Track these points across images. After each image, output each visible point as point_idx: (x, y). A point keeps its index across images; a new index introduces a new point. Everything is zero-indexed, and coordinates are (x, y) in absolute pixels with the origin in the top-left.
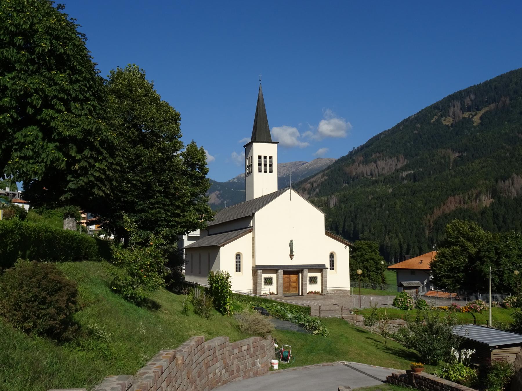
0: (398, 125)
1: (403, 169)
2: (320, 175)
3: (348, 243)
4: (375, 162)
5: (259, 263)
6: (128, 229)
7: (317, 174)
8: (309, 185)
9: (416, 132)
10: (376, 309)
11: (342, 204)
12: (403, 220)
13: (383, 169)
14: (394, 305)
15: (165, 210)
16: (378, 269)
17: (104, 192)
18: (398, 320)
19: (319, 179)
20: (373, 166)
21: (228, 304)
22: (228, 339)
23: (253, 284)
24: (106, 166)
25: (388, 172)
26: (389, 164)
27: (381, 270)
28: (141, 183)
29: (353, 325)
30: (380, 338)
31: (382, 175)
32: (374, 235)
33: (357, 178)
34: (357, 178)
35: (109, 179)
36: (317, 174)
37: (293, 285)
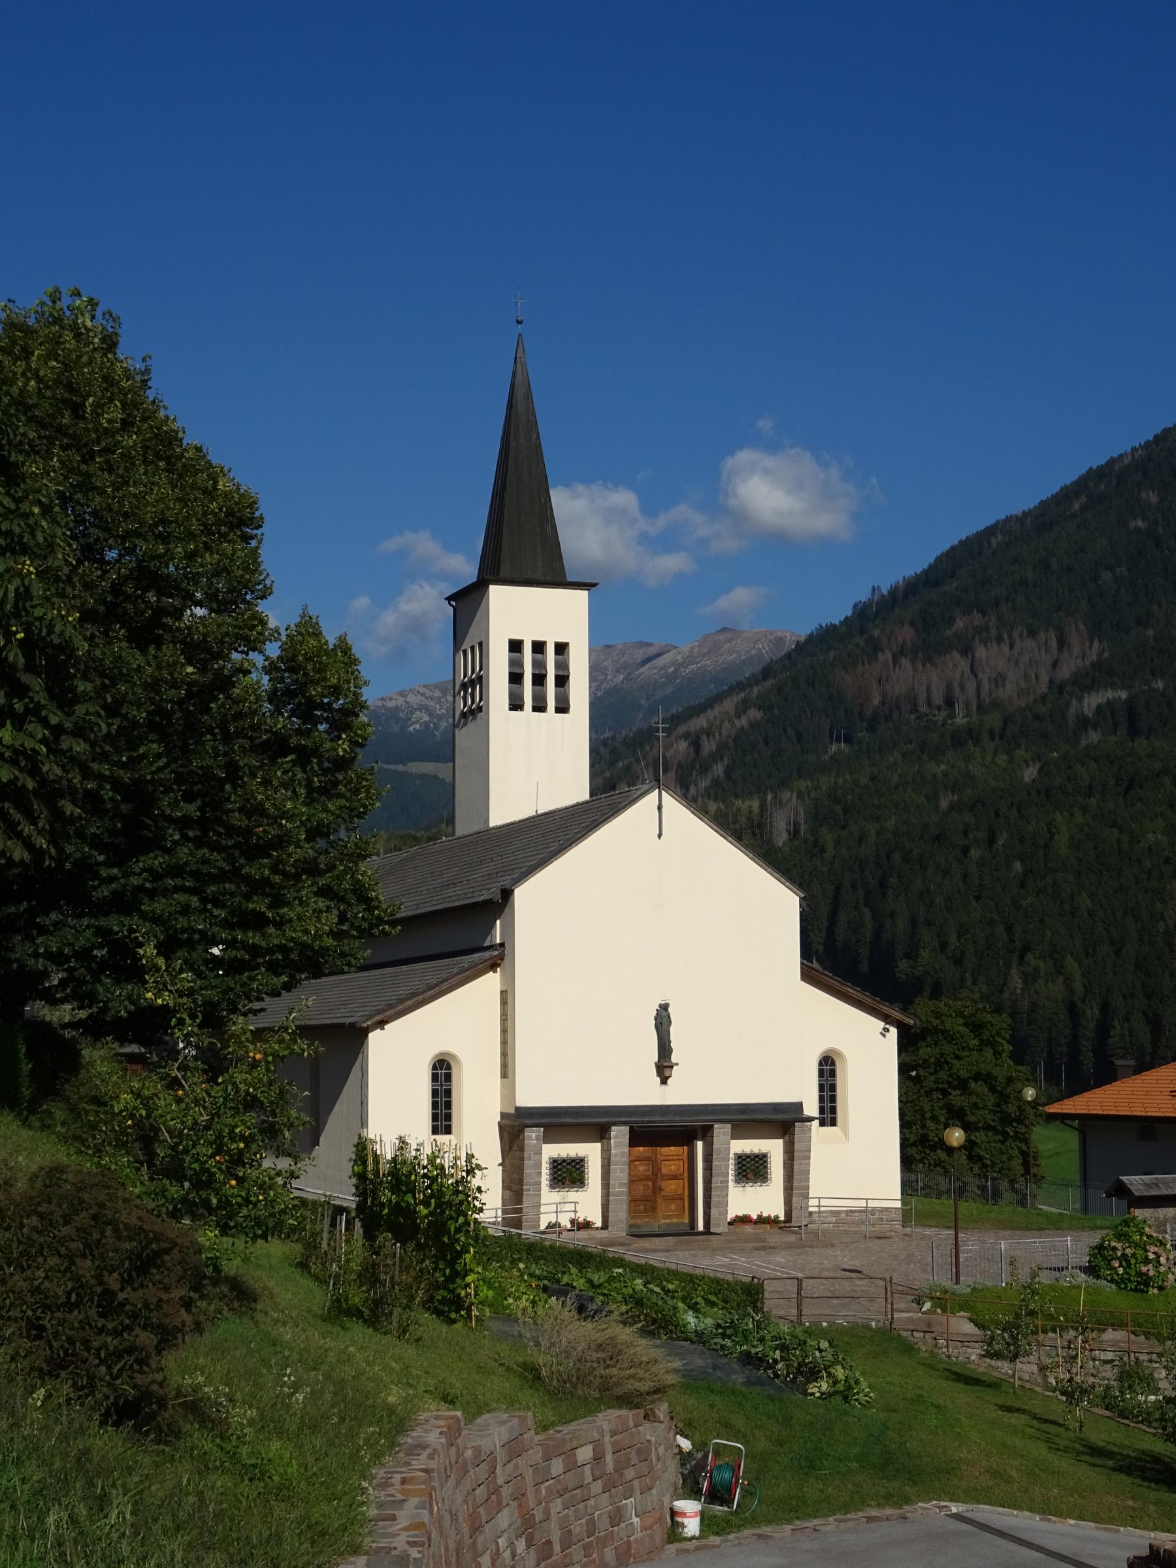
0: (1065, 496)
1: (1086, 682)
2: (729, 705)
3: (897, 1015)
4: (966, 650)
5: (528, 1097)
6: (157, 996)
7: (718, 698)
8: (683, 746)
9: (1140, 524)
10: (1034, 1292)
11: (824, 830)
12: (1085, 901)
13: (999, 680)
14: (1091, 1270)
15: (204, 900)
16: (1006, 1119)
17: (29, 845)
18: (1110, 1335)
19: (728, 719)
20: (955, 665)
21: (469, 1279)
22: (530, 1422)
23: (505, 1187)
24: (44, 741)
25: (1021, 693)
26: (1026, 658)
27: (1020, 1121)
28: (117, 785)
29: (933, 1355)
30: (1057, 1406)
31: (996, 704)
32: (958, 961)
33: (888, 718)
34: (888, 718)
35: (50, 792)
36: (718, 698)
37: (671, 1187)
